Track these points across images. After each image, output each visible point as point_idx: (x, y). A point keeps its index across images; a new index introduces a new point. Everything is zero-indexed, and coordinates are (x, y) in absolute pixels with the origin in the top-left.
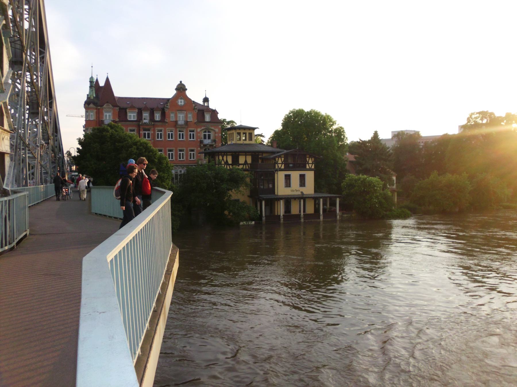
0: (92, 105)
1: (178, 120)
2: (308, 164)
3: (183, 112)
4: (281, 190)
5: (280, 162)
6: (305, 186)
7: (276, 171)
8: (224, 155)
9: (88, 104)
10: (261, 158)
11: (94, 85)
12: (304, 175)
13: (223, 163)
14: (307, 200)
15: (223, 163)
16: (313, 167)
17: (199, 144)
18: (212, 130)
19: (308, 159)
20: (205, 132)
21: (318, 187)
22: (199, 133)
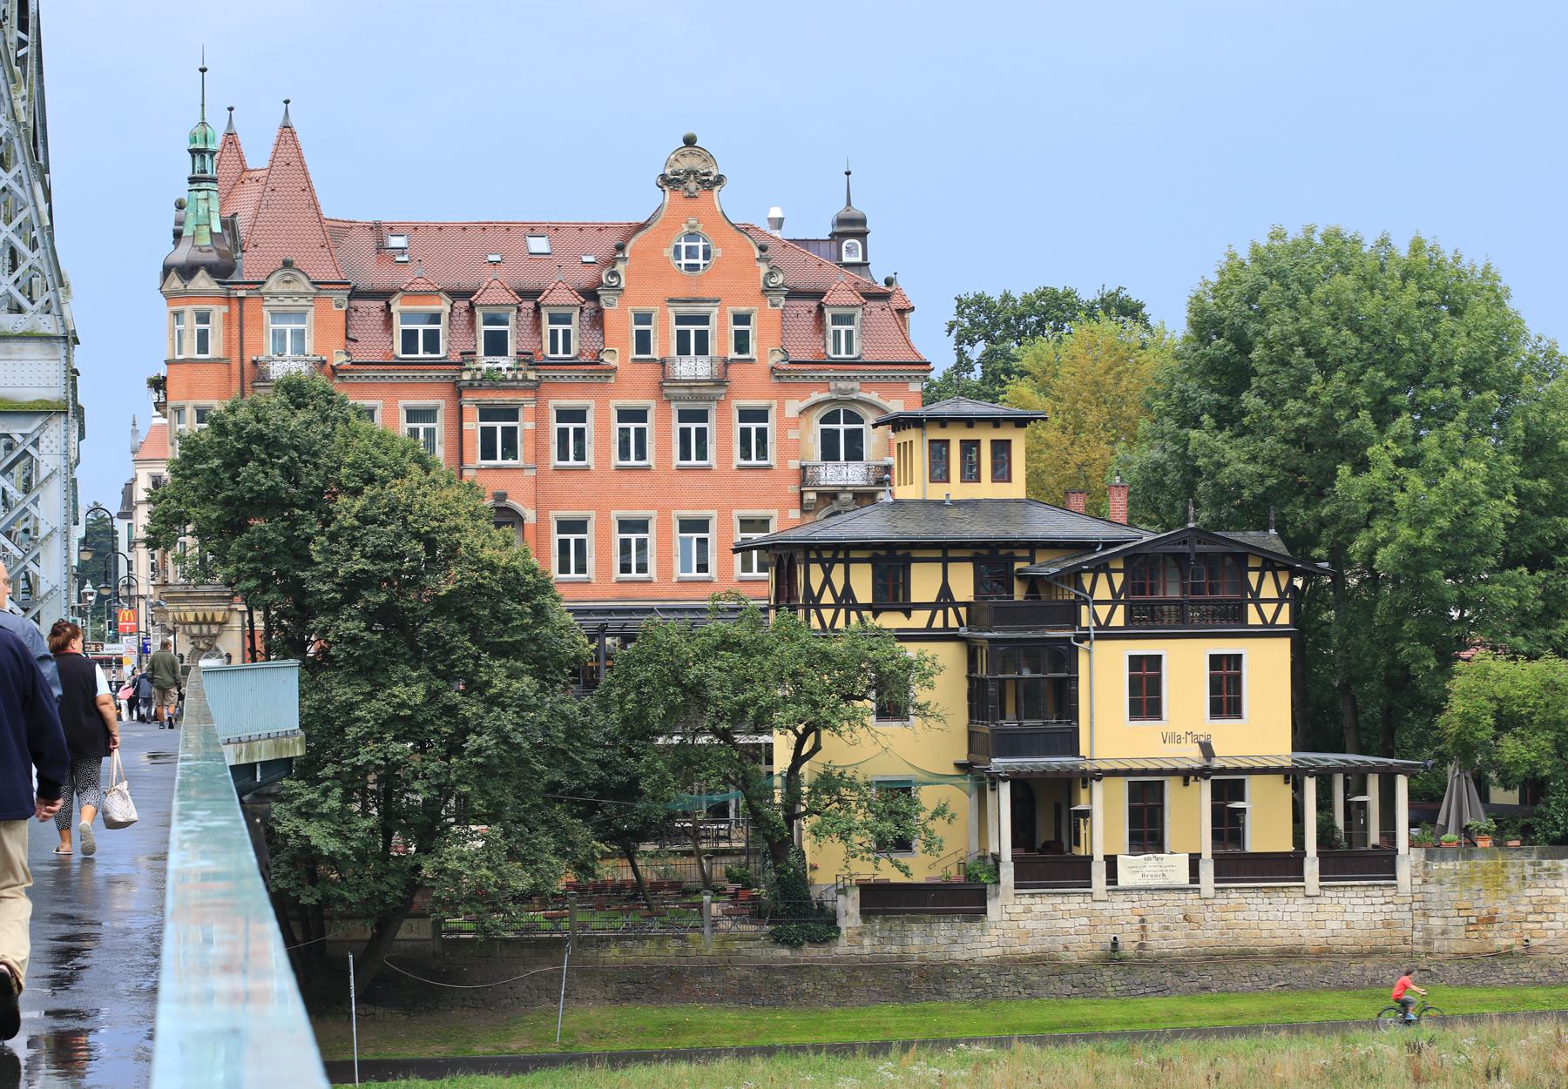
2: (1258, 601)
4: (1108, 732)
5: (1102, 591)
7: (1080, 639)
11: (208, 161)
12: (1238, 657)
13: (827, 598)
15: (827, 598)
16: (1284, 618)
17: (793, 489)
18: (188, 598)
19: (1253, 577)
20: (831, 418)
21: (1312, 724)
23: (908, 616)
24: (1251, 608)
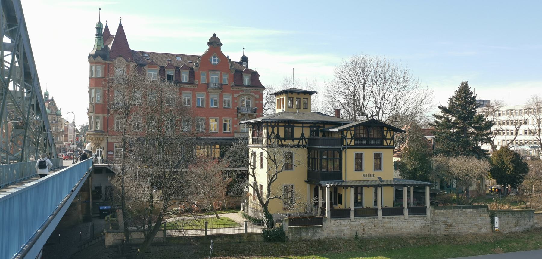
0: (99, 59)
1: (210, 82)
2: (386, 139)
3: (217, 72)
4: (350, 174)
5: (349, 136)
6: (355, 170)
7: (343, 149)
8: (275, 126)
9: (92, 58)
10: (321, 131)
11: (102, 33)
12: (362, 154)
13: (273, 136)
14: (364, 188)
19: (385, 133)
22: (236, 99)
23: (293, 141)
24: (384, 141)
